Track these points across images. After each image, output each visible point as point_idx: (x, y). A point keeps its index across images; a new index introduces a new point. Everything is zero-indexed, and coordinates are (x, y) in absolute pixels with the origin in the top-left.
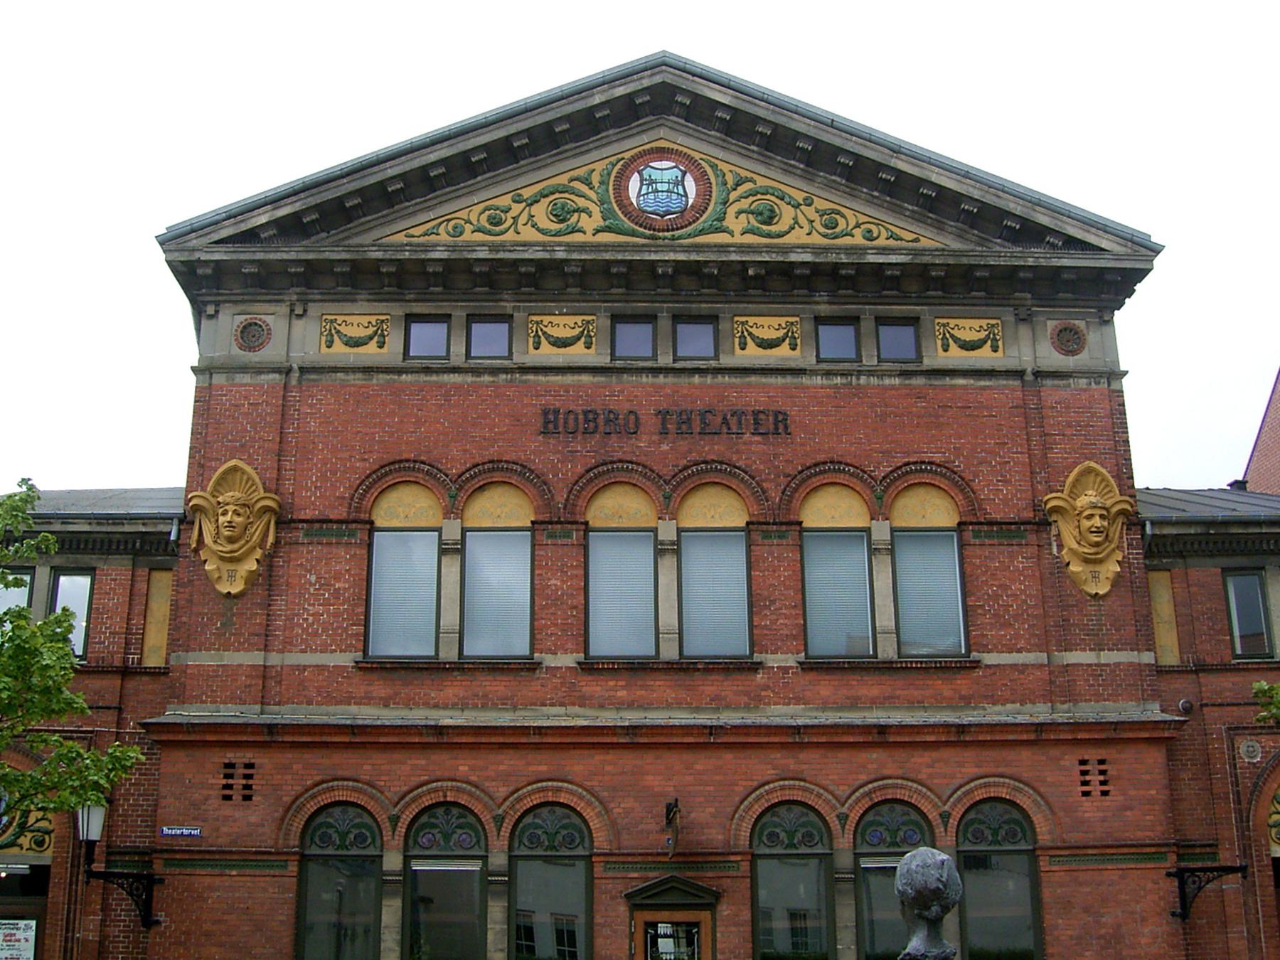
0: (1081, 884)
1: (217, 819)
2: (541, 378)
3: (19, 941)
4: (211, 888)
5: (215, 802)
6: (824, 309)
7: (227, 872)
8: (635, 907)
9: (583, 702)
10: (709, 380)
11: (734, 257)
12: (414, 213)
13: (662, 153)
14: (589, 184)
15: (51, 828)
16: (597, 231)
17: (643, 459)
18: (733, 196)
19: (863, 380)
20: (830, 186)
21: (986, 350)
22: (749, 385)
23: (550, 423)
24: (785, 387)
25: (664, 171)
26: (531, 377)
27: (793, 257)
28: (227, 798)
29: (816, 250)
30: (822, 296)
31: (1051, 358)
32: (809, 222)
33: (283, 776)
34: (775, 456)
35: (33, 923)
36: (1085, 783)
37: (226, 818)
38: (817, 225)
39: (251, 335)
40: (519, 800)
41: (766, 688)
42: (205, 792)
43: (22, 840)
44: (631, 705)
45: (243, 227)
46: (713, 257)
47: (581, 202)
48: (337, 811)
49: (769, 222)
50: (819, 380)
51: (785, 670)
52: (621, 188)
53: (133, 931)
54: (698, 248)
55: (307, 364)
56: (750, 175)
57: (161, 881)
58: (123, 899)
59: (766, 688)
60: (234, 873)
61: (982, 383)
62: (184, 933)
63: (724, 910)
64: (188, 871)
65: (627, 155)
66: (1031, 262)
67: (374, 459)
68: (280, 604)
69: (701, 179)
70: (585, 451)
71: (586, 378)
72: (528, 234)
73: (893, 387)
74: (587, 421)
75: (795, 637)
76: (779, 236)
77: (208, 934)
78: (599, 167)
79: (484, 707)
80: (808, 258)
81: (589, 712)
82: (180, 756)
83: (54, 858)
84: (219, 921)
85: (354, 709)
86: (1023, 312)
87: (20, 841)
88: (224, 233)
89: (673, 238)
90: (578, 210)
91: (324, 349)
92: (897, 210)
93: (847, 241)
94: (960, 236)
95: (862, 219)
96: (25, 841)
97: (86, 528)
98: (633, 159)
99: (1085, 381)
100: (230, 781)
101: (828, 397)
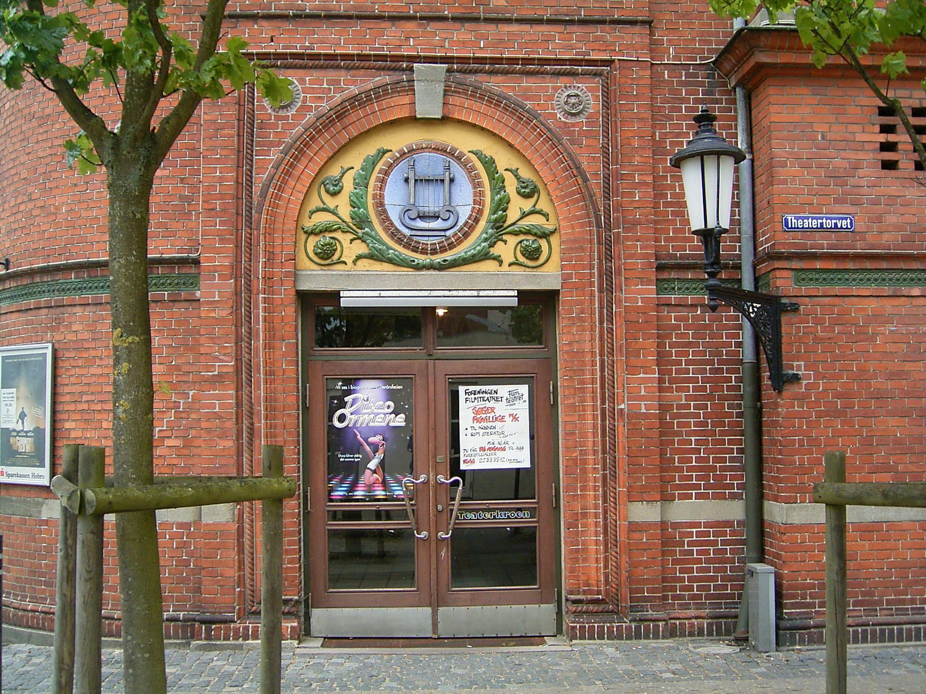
1: (876, 203)
3: (502, 419)
5: (870, 171)
7: (905, 291)
15: (549, 226)
28: (889, 165)
35: (524, 389)
36: (887, 147)
37: (892, 200)
42: (852, 155)
43: (499, 249)
53: (710, 397)
57: (795, 308)
58: (689, 344)
60: (916, 291)
62: (839, 396)
64: (837, 289)
77: (879, 396)
83: (566, 278)
84: (899, 375)
87: (495, 251)
96: (507, 249)
100: (892, 138)
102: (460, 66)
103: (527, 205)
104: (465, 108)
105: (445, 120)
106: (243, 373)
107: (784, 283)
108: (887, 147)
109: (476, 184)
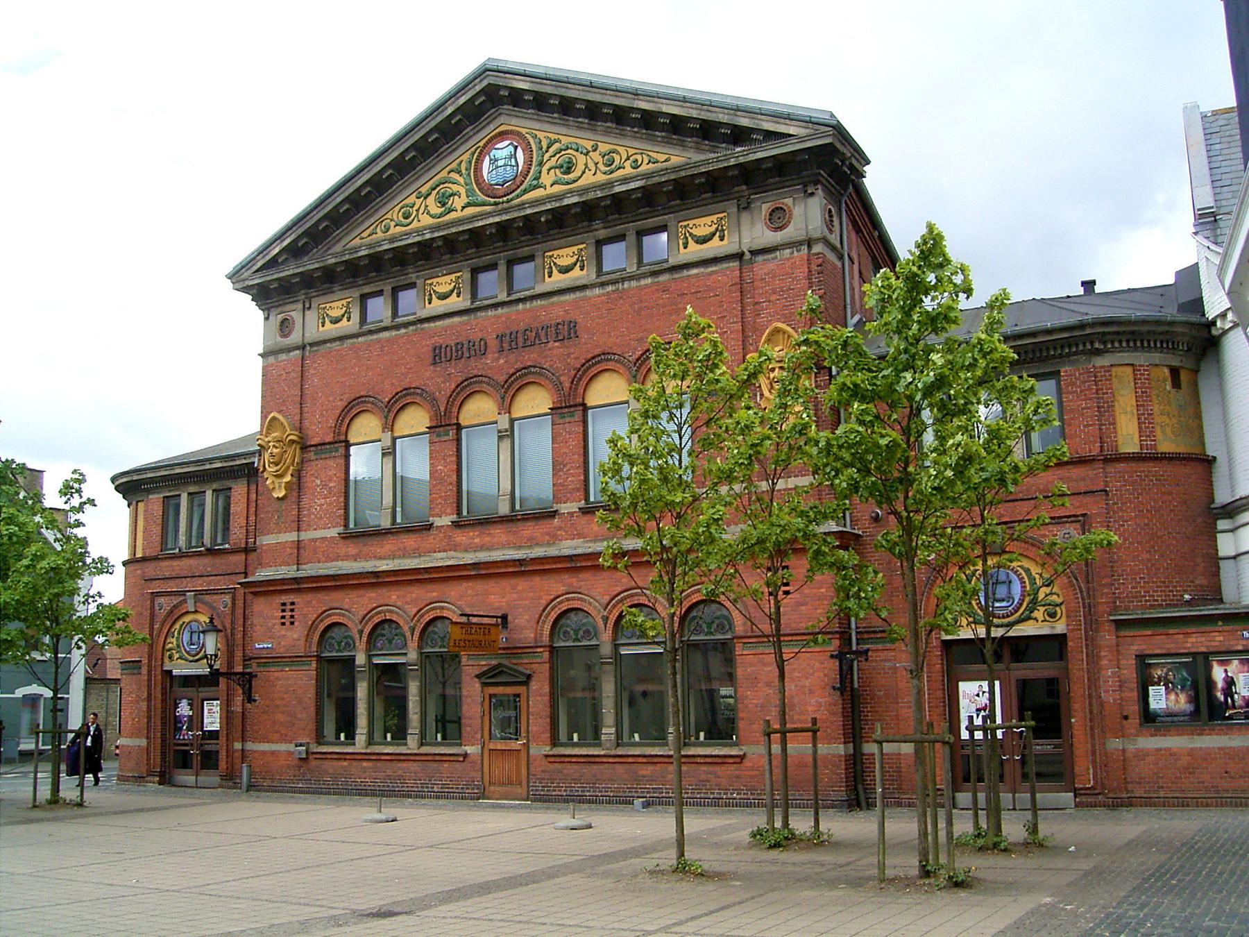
0: (764, 665)
2: (432, 325)
4: (278, 679)
5: (278, 627)
6: (602, 234)
8: (484, 685)
9: (455, 547)
10: (528, 305)
11: (529, 211)
12: (363, 222)
13: (502, 135)
14: (459, 172)
15: (1059, 600)
16: (463, 208)
17: (489, 373)
18: (547, 156)
19: (626, 285)
20: (607, 132)
21: (716, 241)
22: (553, 304)
23: (439, 355)
24: (575, 301)
25: (503, 150)
26: (426, 325)
27: (566, 202)
28: (283, 624)
29: (602, 186)
30: (598, 224)
31: (770, 237)
32: (603, 163)
33: (309, 607)
34: (569, 355)
36: (283, 617)
38: (601, 166)
39: (285, 327)
40: (422, 616)
41: (560, 528)
44: (482, 548)
45: (268, 258)
46: (516, 215)
47: (455, 188)
48: (572, 615)
49: (568, 171)
50: (597, 291)
51: (571, 514)
52: (478, 170)
54: (521, 206)
55: (755, 247)
56: (556, 137)
59: (560, 528)
61: (710, 269)
63: (534, 685)
65: (481, 144)
66: (732, 162)
67: (347, 398)
68: (305, 501)
69: (528, 150)
70: (456, 372)
71: (456, 319)
72: (426, 220)
73: (646, 286)
74: (457, 351)
75: (578, 490)
76: (575, 181)
77: (277, 706)
78: (465, 157)
79: (404, 557)
80: (575, 199)
81: (459, 555)
82: (262, 600)
85: (340, 563)
86: (743, 203)
87: (1033, 615)
88: (259, 264)
89: (508, 201)
90: (453, 195)
91: (321, 329)
92: (652, 139)
93: (620, 173)
94: (698, 149)
95: (631, 151)
97: (219, 465)
98: (485, 146)
99: (788, 251)
101: (602, 303)
102: (198, 593)
103: (1047, 590)
104: (201, 607)
105: (196, 612)
106: (149, 698)
107: (254, 668)
108: (283, 617)
109: (1021, 579)
